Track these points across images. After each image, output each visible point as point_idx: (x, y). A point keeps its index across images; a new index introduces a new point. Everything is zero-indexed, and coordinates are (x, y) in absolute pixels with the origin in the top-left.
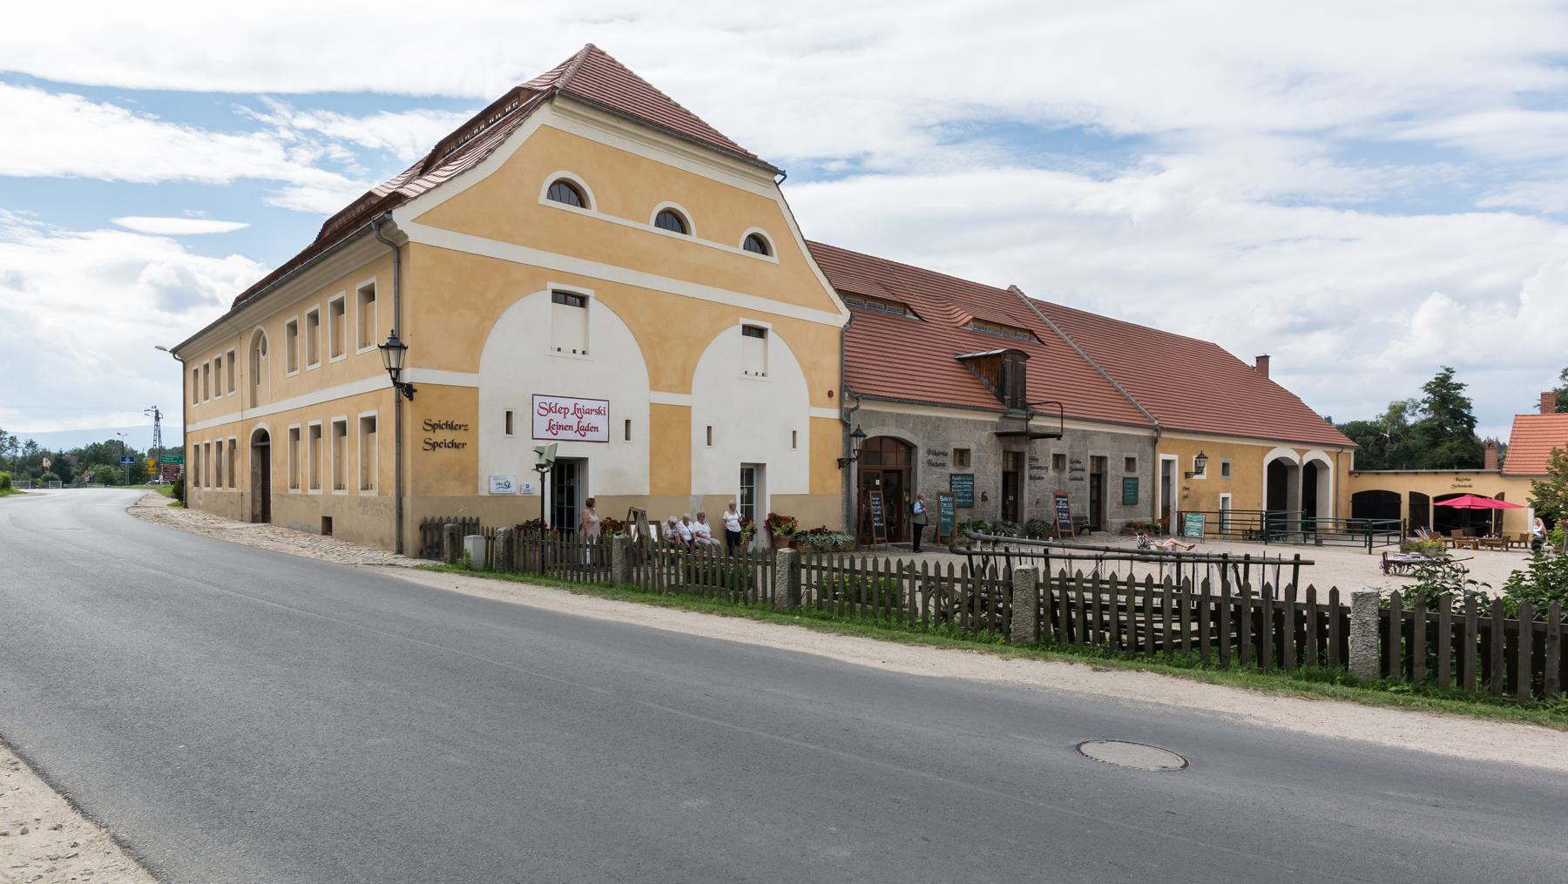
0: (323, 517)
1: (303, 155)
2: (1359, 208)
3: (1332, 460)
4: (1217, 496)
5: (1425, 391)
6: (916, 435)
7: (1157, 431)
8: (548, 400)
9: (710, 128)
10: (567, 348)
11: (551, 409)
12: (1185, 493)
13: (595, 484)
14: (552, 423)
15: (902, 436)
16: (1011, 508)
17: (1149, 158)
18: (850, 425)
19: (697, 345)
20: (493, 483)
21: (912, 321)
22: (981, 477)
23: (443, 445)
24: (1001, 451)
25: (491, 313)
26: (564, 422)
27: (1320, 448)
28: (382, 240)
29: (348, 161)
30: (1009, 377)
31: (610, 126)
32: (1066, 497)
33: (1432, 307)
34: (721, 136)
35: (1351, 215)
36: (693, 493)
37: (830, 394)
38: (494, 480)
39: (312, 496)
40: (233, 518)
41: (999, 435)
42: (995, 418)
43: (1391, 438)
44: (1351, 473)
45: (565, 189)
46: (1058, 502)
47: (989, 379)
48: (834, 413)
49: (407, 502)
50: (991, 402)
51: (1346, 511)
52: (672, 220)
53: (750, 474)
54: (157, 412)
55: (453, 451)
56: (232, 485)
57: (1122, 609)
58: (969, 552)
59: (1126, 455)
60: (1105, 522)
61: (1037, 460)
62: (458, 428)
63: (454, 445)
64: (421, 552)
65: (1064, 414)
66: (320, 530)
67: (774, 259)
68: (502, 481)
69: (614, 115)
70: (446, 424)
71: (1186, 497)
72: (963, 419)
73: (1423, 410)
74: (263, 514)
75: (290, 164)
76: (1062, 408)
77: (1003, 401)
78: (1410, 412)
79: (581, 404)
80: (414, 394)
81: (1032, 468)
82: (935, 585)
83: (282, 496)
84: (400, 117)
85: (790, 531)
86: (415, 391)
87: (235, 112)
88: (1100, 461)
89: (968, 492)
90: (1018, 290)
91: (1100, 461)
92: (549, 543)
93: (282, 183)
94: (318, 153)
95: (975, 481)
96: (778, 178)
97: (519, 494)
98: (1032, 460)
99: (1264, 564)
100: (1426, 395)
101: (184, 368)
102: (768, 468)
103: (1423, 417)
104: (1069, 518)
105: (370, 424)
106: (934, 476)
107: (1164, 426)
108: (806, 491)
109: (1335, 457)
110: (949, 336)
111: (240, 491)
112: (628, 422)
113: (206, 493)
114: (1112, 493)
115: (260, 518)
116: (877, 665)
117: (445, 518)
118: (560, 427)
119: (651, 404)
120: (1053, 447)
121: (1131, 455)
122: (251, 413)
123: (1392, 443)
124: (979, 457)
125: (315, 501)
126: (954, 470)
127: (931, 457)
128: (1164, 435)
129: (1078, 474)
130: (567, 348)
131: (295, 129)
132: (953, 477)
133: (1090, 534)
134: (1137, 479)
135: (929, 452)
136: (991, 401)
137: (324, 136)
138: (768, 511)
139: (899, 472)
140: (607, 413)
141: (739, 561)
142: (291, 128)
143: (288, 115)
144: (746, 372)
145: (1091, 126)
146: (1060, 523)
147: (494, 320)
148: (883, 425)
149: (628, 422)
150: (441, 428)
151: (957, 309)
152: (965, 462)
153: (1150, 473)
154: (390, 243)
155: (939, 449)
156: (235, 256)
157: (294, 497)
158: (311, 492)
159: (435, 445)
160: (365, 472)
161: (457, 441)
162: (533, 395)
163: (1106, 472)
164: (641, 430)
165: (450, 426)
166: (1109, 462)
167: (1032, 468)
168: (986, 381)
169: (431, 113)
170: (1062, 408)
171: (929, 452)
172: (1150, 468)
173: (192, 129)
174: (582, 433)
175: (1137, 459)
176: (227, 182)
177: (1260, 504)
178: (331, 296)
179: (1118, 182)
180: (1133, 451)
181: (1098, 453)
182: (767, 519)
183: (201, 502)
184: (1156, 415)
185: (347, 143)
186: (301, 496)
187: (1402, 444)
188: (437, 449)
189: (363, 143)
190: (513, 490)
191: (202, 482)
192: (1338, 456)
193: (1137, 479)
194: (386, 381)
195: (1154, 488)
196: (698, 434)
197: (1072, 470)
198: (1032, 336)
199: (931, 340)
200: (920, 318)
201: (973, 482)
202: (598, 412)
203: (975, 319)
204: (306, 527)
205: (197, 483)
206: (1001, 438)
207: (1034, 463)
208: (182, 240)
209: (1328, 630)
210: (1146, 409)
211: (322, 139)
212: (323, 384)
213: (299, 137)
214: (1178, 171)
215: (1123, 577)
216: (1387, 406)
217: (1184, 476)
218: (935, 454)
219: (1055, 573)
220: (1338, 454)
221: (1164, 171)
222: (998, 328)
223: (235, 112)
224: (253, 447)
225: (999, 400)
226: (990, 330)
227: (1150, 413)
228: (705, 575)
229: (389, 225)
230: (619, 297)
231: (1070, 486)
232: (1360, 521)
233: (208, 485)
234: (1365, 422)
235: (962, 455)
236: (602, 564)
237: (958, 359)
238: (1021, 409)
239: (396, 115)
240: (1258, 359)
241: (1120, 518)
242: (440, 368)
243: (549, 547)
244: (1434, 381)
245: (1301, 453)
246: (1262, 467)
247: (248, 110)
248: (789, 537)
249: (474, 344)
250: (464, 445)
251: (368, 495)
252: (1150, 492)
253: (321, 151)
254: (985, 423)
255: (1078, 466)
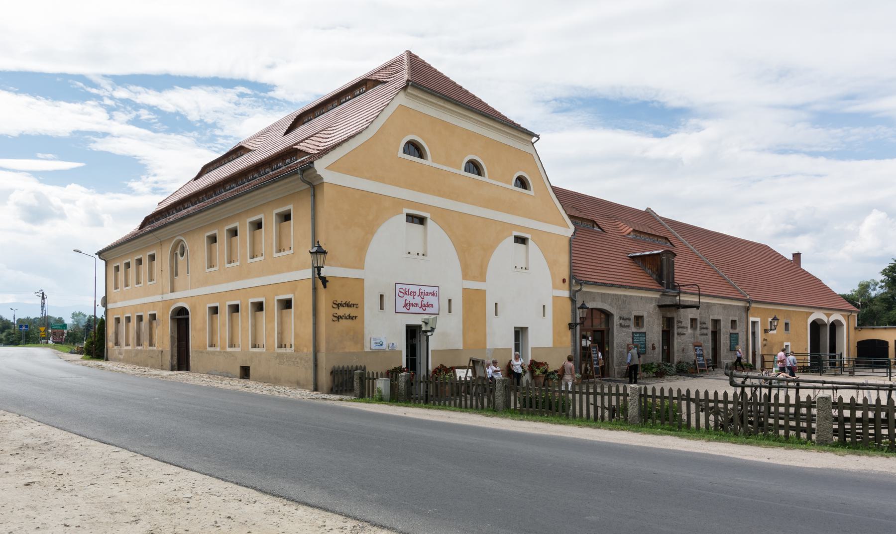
0: (241, 367)
1: (121, 116)
2: (828, 155)
3: (846, 320)
4: (782, 344)
5: (883, 275)
6: (613, 307)
7: (749, 302)
8: (404, 287)
9: (489, 107)
10: (414, 252)
11: (405, 292)
12: (765, 342)
13: (435, 343)
14: (407, 302)
15: (605, 308)
16: (667, 354)
17: (693, 121)
18: (576, 301)
19: (489, 249)
20: (373, 342)
21: (598, 232)
22: (650, 334)
23: (343, 318)
24: (661, 317)
25: (370, 229)
26: (413, 302)
27: (837, 312)
28: (304, 181)
29: (153, 121)
30: (665, 268)
31: (439, 105)
32: (701, 346)
33: (872, 220)
34: (497, 112)
35: (822, 160)
36: (487, 347)
37: (564, 281)
38: (374, 340)
39: (231, 352)
40: (153, 367)
41: (660, 306)
42: (656, 295)
43: (862, 305)
44: (856, 328)
45: (412, 148)
46: (696, 349)
47: (651, 269)
48: (566, 294)
49: (322, 357)
50: (655, 286)
51: (854, 354)
52: (474, 167)
53: (520, 333)
54: (43, 294)
55: (350, 321)
56: (151, 344)
57: (847, 420)
58: (743, 385)
59: (731, 318)
60: (720, 362)
61: (705, 323)
62: (352, 306)
63: (351, 318)
64: (332, 390)
65: (700, 292)
66: (239, 375)
67: (531, 193)
68: (378, 341)
69: (443, 99)
70: (345, 304)
71: (765, 345)
72: (639, 296)
73: (881, 287)
74: (182, 361)
75: (111, 121)
76: (699, 288)
77: (662, 284)
78: (872, 288)
79: (423, 289)
80: (327, 284)
81: (678, 328)
82: (704, 404)
83: (201, 352)
84: (189, 90)
85: (546, 371)
86: (328, 281)
87: (72, 86)
88: (716, 322)
89: (643, 344)
90: (652, 211)
91: (716, 322)
92: (431, 382)
93: (105, 135)
94: (131, 115)
95: (647, 337)
96: (534, 139)
97: (387, 350)
98: (679, 322)
99: (787, 388)
100: (883, 277)
101: (106, 265)
102: (530, 331)
103: (882, 291)
104: (703, 360)
105: (287, 304)
106: (623, 334)
107: (753, 299)
108: (551, 345)
109: (847, 319)
110: (621, 241)
111: (161, 349)
112: (450, 301)
113: (126, 351)
114: (724, 344)
115: (176, 367)
116: (765, 460)
117: (354, 366)
118: (411, 305)
119: (463, 288)
120: (691, 313)
121: (734, 319)
122: (170, 296)
123: (862, 308)
124: (649, 321)
125: (233, 356)
126: (634, 330)
127: (621, 321)
128: (753, 305)
129: (705, 331)
130: (414, 252)
131: (116, 99)
132: (634, 334)
133: (714, 370)
134: (738, 334)
135: (621, 318)
136: (653, 284)
137: (136, 104)
138: (530, 359)
139: (602, 332)
140: (438, 295)
141: (549, 391)
142: (112, 98)
143: (110, 89)
144: (516, 267)
145: (653, 102)
146: (698, 364)
147: (373, 234)
148: (594, 301)
149: (450, 301)
150: (343, 306)
151: (622, 224)
152: (640, 324)
153: (744, 330)
154: (309, 183)
155: (626, 317)
156: (73, 185)
157: (214, 353)
158: (229, 349)
159: (339, 318)
160: (280, 335)
161: (352, 315)
162: (396, 283)
163: (720, 330)
164: (458, 306)
165: (348, 305)
166: (722, 323)
167: (678, 328)
168: (649, 271)
169: (210, 88)
170: (699, 288)
171: (621, 318)
172: (745, 326)
173: (41, 98)
174: (424, 308)
175: (737, 321)
176: (68, 135)
177: (806, 349)
178: (249, 217)
179: (673, 137)
180: (735, 316)
181: (716, 318)
182: (529, 364)
183: (121, 357)
184: (748, 293)
185: (151, 109)
186: (220, 352)
187: (868, 308)
188: (340, 320)
189: (162, 109)
190: (384, 347)
191: (122, 341)
192: (848, 317)
193: (738, 334)
194: (308, 273)
195: (747, 340)
196: (490, 308)
197: (701, 328)
198: (667, 241)
199: (597, 244)
200: (603, 230)
201: (645, 337)
202: (433, 294)
203: (634, 231)
204: (225, 374)
205: (117, 343)
206: (661, 308)
207: (680, 324)
208: (35, 174)
209: (814, 429)
210: (741, 288)
211: (134, 106)
212: (241, 275)
213: (118, 104)
214: (712, 130)
215: (847, 400)
216: (858, 283)
217: (764, 332)
218: (624, 319)
219: (803, 399)
220: (848, 316)
221: (703, 130)
222: (647, 236)
223: (72, 86)
224: (172, 318)
225: (660, 284)
226: (643, 237)
227: (744, 291)
228: (537, 403)
229: (310, 171)
230: (446, 218)
231: (700, 339)
232: (864, 359)
233: (128, 345)
234: (845, 295)
235: (639, 320)
236: (437, 396)
237: (629, 257)
238: (672, 289)
239: (185, 90)
240: (794, 255)
241: (728, 359)
242: (342, 266)
243: (431, 385)
244: (888, 268)
245: (828, 316)
246: (807, 325)
247: (81, 84)
248: (544, 375)
249: (362, 248)
250: (356, 317)
251: (285, 351)
252: (745, 342)
253: (134, 113)
254: (652, 298)
255: (704, 326)
